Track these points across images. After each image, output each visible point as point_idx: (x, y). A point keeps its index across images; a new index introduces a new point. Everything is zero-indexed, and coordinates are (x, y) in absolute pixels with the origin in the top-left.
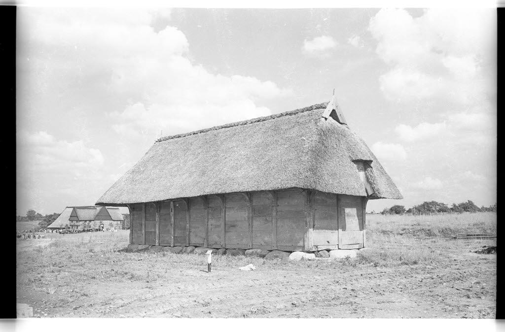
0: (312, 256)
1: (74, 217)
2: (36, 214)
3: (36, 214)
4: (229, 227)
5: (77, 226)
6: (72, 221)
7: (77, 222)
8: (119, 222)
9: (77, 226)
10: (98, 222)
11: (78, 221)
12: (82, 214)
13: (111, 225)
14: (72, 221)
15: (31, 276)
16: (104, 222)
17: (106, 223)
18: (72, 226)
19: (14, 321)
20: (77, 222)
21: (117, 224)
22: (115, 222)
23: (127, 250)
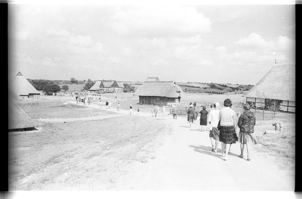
0: (168, 106)
1: (102, 85)
2: (75, 80)
3: (75, 80)
4: (157, 101)
5: (103, 90)
6: (101, 87)
7: (103, 88)
8: (122, 89)
9: (103, 90)
10: (113, 88)
11: (104, 87)
12: (105, 84)
13: (118, 90)
14: (101, 87)
15: (290, 83)
16: (115, 88)
17: (116, 89)
18: (101, 90)
19: (7, 193)
20: (103, 88)
21: (121, 90)
22: (120, 89)
23: (138, 104)
